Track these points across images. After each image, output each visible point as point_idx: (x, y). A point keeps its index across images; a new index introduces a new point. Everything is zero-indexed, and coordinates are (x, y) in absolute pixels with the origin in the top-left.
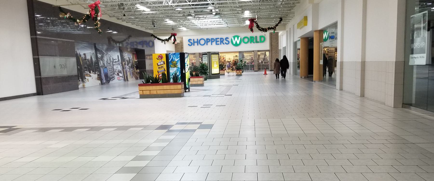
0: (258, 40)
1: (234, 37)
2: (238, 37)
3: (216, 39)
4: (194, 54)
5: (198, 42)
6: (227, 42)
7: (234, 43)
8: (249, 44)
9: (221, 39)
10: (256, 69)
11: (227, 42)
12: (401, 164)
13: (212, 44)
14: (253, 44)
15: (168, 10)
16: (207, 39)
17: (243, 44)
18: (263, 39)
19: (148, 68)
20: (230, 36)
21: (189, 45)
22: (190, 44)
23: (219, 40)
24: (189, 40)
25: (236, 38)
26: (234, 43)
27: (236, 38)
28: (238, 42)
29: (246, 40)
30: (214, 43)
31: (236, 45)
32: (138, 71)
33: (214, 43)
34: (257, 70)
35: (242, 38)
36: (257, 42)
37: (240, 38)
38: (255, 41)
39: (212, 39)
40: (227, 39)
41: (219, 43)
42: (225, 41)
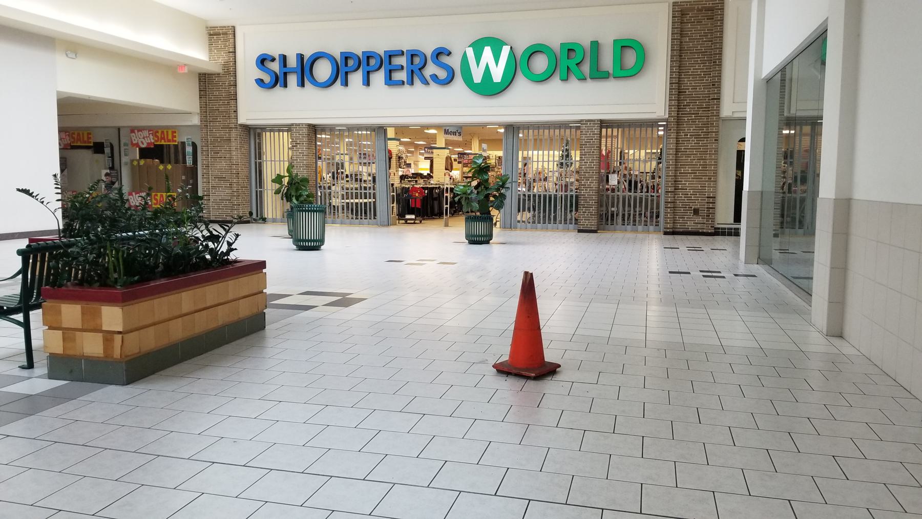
0: (608, 62)
1: (478, 46)
2: (496, 44)
3: (391, 55)
4: (289, 128)
5: (305, 69)
6: (442, 74)
7: (477, 78)
8: (556, 84)
9: (413, 55)
10: (588, 217)
11: (442, 74)
12: (858, 391)
13: (367, 83)
14: (574, 85)
15: (635, 211)
16: (346, 57)
17: (522, 85)
18: (631, 58)
19: (726, 110)
20: (461, 47)
21: (260, 82)
22: (267, 79)
23: (402, 61)
24: (263, 61)
25: (487, 52)
26: (477, 78)
27: (487, 52)
28: (498, 74)
29: (541, 64)
30: (378, 78)
31: (489, 89)
32: (337, 158)
33: (378, 78)
34: (593, 223)
35: (519, 52)
36: (599, 75)
37: (506, 50)
38: (586, 68)
39: (369, 56)
40: (445, 59)
41: (402, 76)
42: (431, 69)
